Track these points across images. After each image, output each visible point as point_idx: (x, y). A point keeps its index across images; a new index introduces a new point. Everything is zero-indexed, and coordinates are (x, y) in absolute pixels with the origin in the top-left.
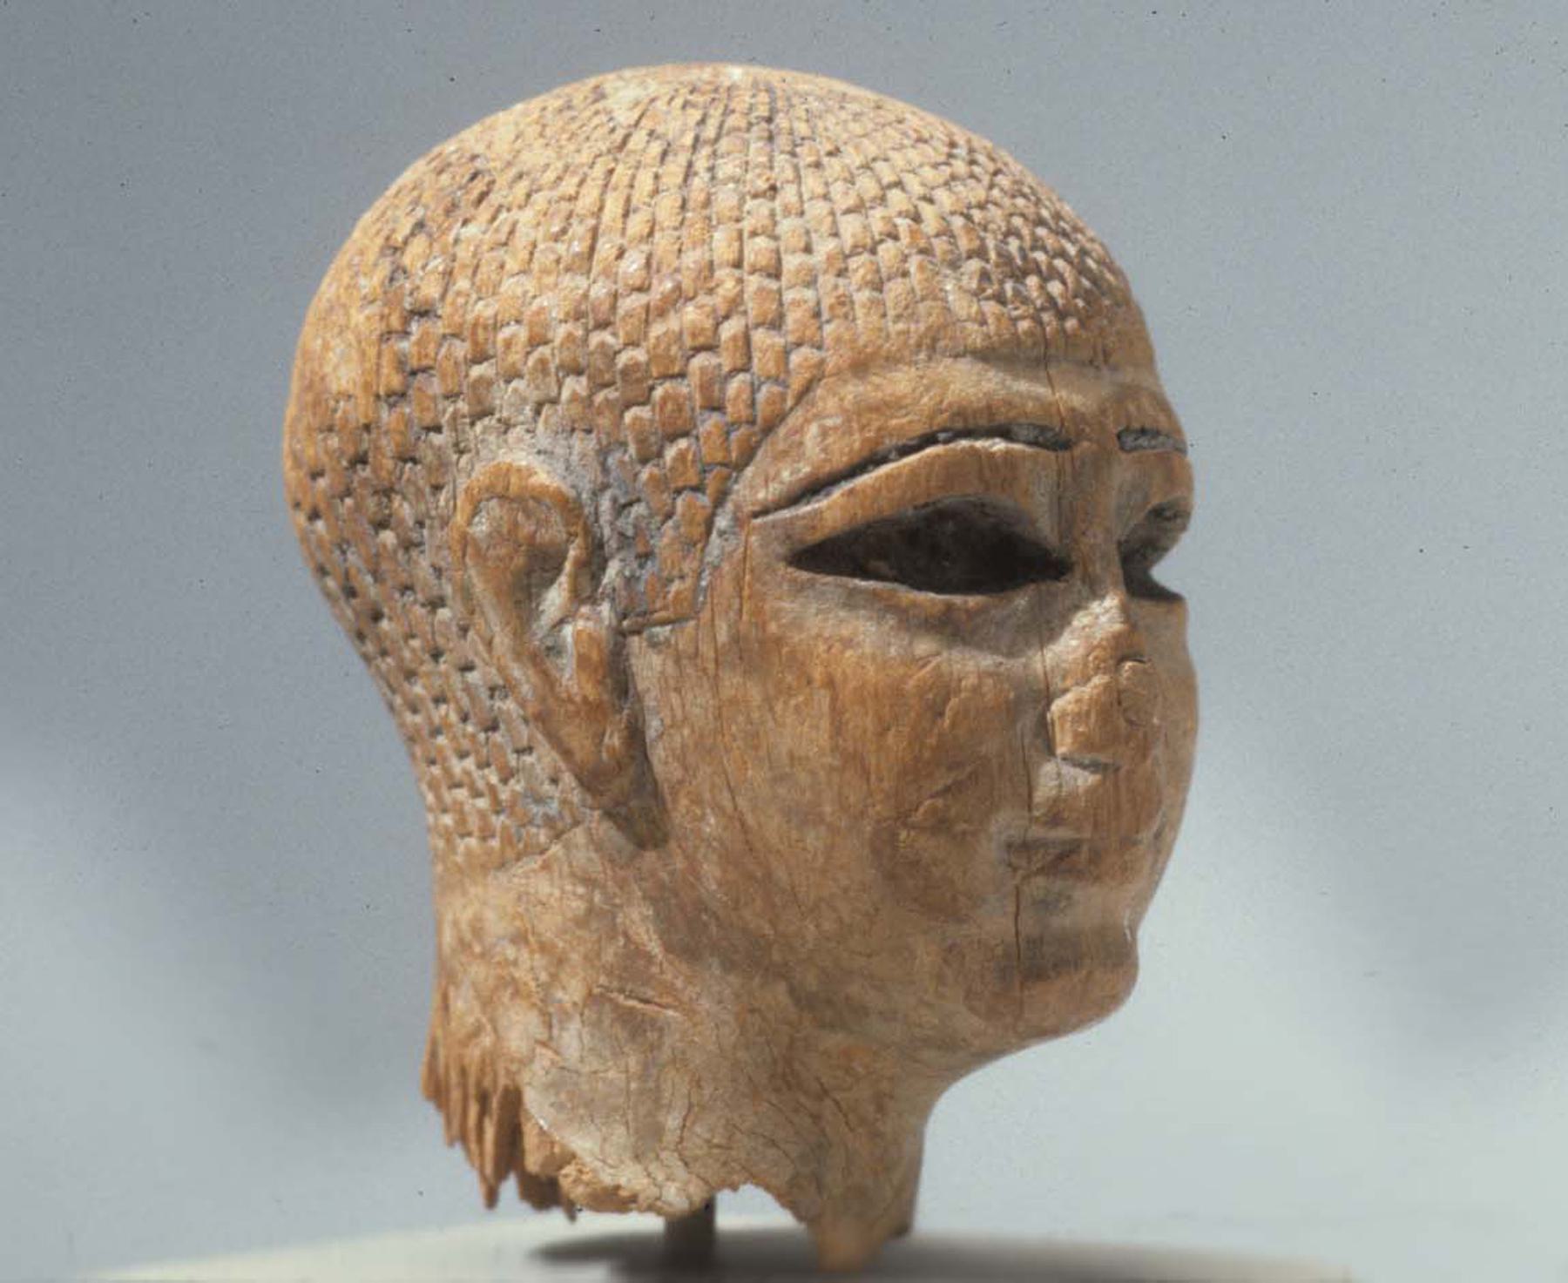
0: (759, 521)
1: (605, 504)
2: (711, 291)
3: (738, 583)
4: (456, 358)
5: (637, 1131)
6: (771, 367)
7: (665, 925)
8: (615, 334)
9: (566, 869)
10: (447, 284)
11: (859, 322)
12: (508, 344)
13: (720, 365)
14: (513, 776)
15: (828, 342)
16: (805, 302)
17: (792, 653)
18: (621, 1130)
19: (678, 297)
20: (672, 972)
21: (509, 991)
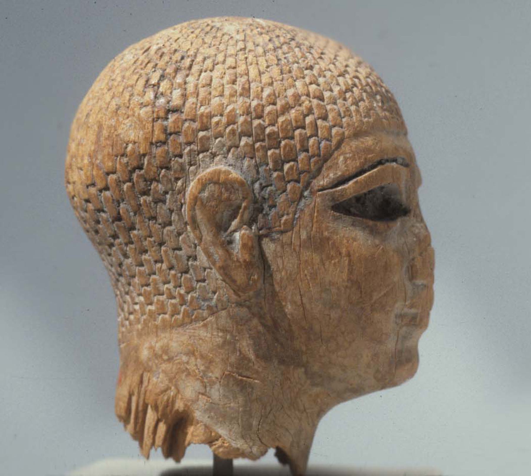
0: (320, 193)
1: (257, 186)
2: (300, 105)
3: (312, 217)
4: (193, 128)
5: (243, 427)
6: (326, 134)
8: (264, 121)
9: (215, 326)
10: (185, 99)
11: (354, 118)
12: (217, 123)
13: (306, 133)
15: (345, 125)
16: (335, 110)
17: (334, 243)
18: (236, 426)
19: (286, 109)
21: (185, 373)
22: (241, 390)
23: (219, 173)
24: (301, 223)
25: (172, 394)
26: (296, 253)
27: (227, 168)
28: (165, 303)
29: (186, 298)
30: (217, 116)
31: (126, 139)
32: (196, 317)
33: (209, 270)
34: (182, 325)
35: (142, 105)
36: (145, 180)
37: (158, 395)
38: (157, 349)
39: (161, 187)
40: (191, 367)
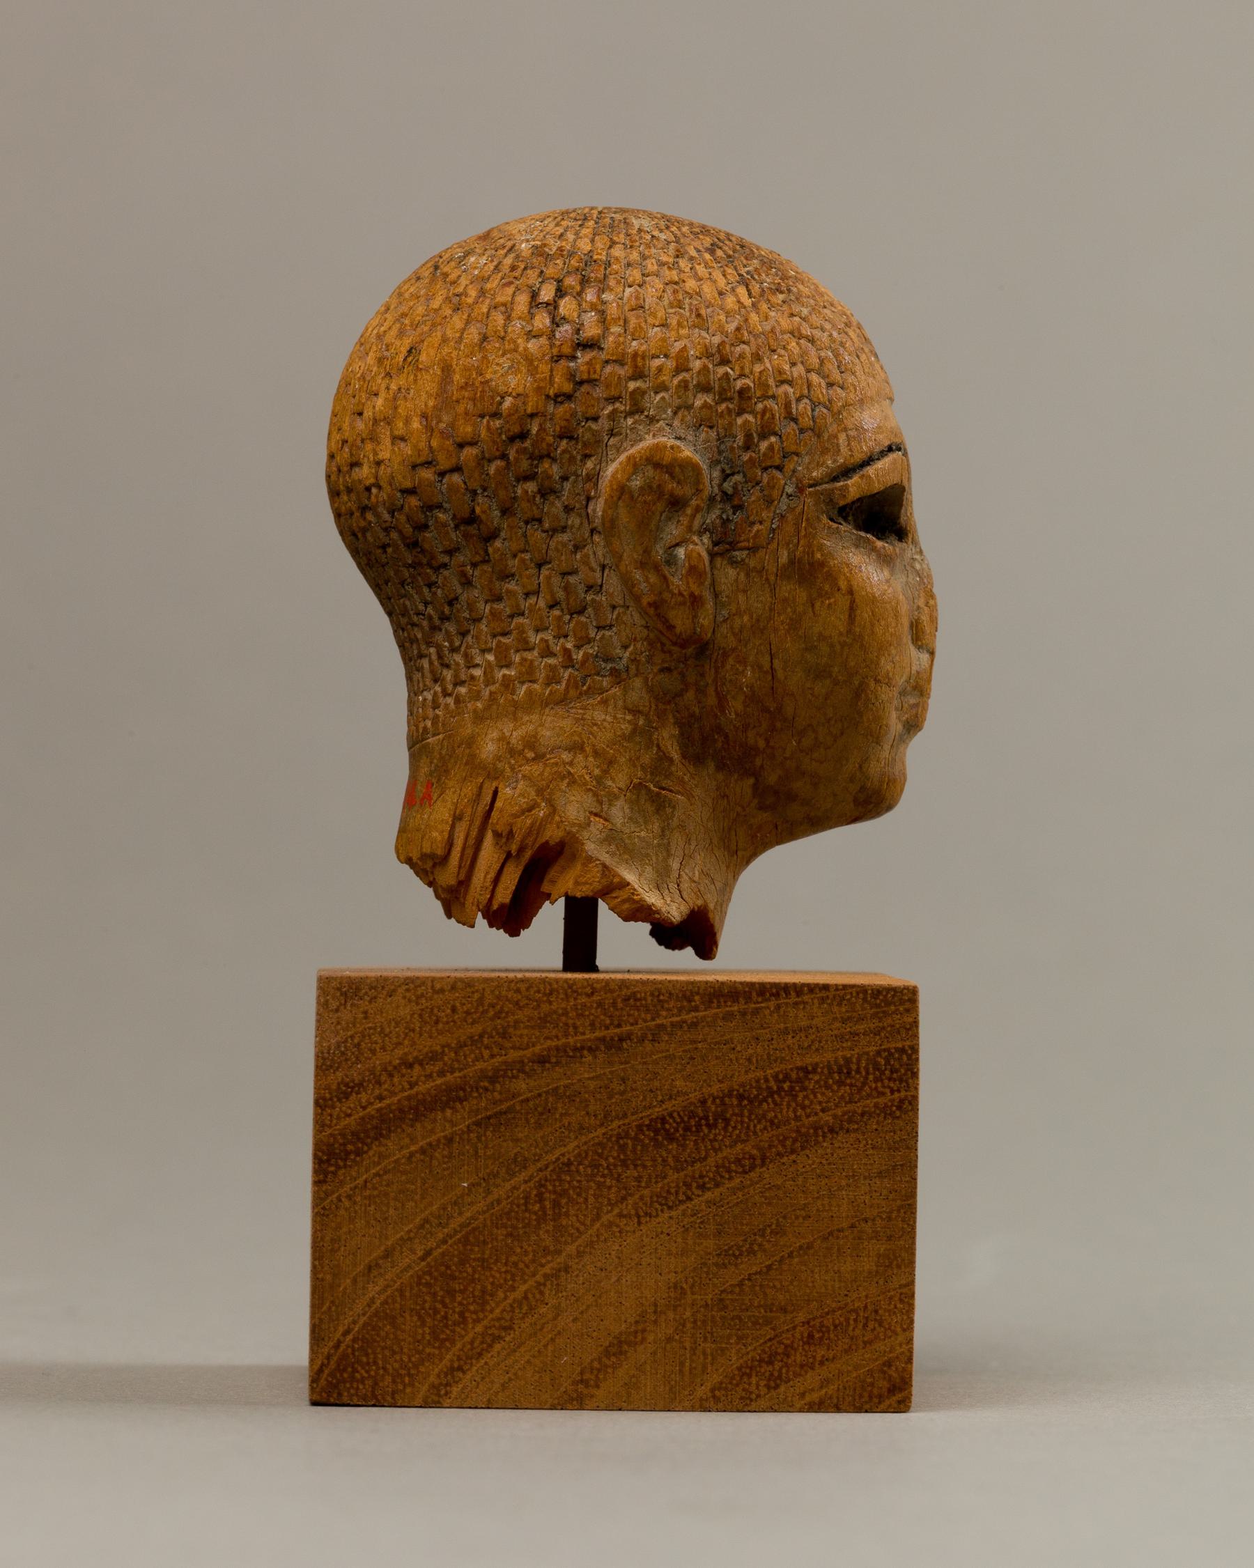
7: (685, 740)
9: (620, 703)
14: (589, 643)
18: (649, 869)
20: (680, 768)
22: (657, 811)
23: (658, 448)
24: (780, 538)
25: (541, 814)
26: (770, 585)
27: (672, 442)
28: (536, 663)
29: (575, 657)
30: (658, 357)
31: (502, 389)
32: (589, 688)
33: (621, 610)
34: (563, 701)
35: (530, 335)
36: (531, 458)
37: (516, 816)
38: (513, 741)
39: (555, 470)
40: (578, 770)
